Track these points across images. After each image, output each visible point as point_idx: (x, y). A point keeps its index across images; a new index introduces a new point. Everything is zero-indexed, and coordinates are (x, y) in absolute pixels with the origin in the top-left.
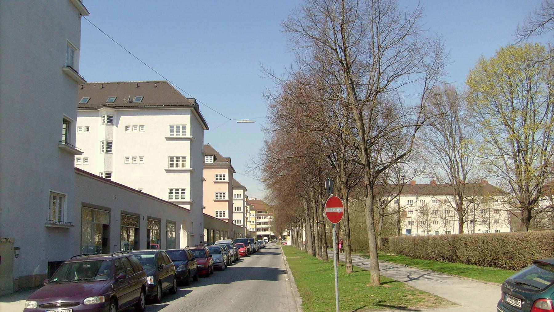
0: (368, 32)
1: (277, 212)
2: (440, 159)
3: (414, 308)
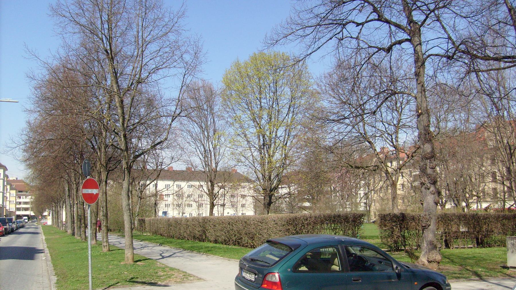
0: (134, 26)
1: (37, 192)
2: (195, 148)
3: (163, 283)
